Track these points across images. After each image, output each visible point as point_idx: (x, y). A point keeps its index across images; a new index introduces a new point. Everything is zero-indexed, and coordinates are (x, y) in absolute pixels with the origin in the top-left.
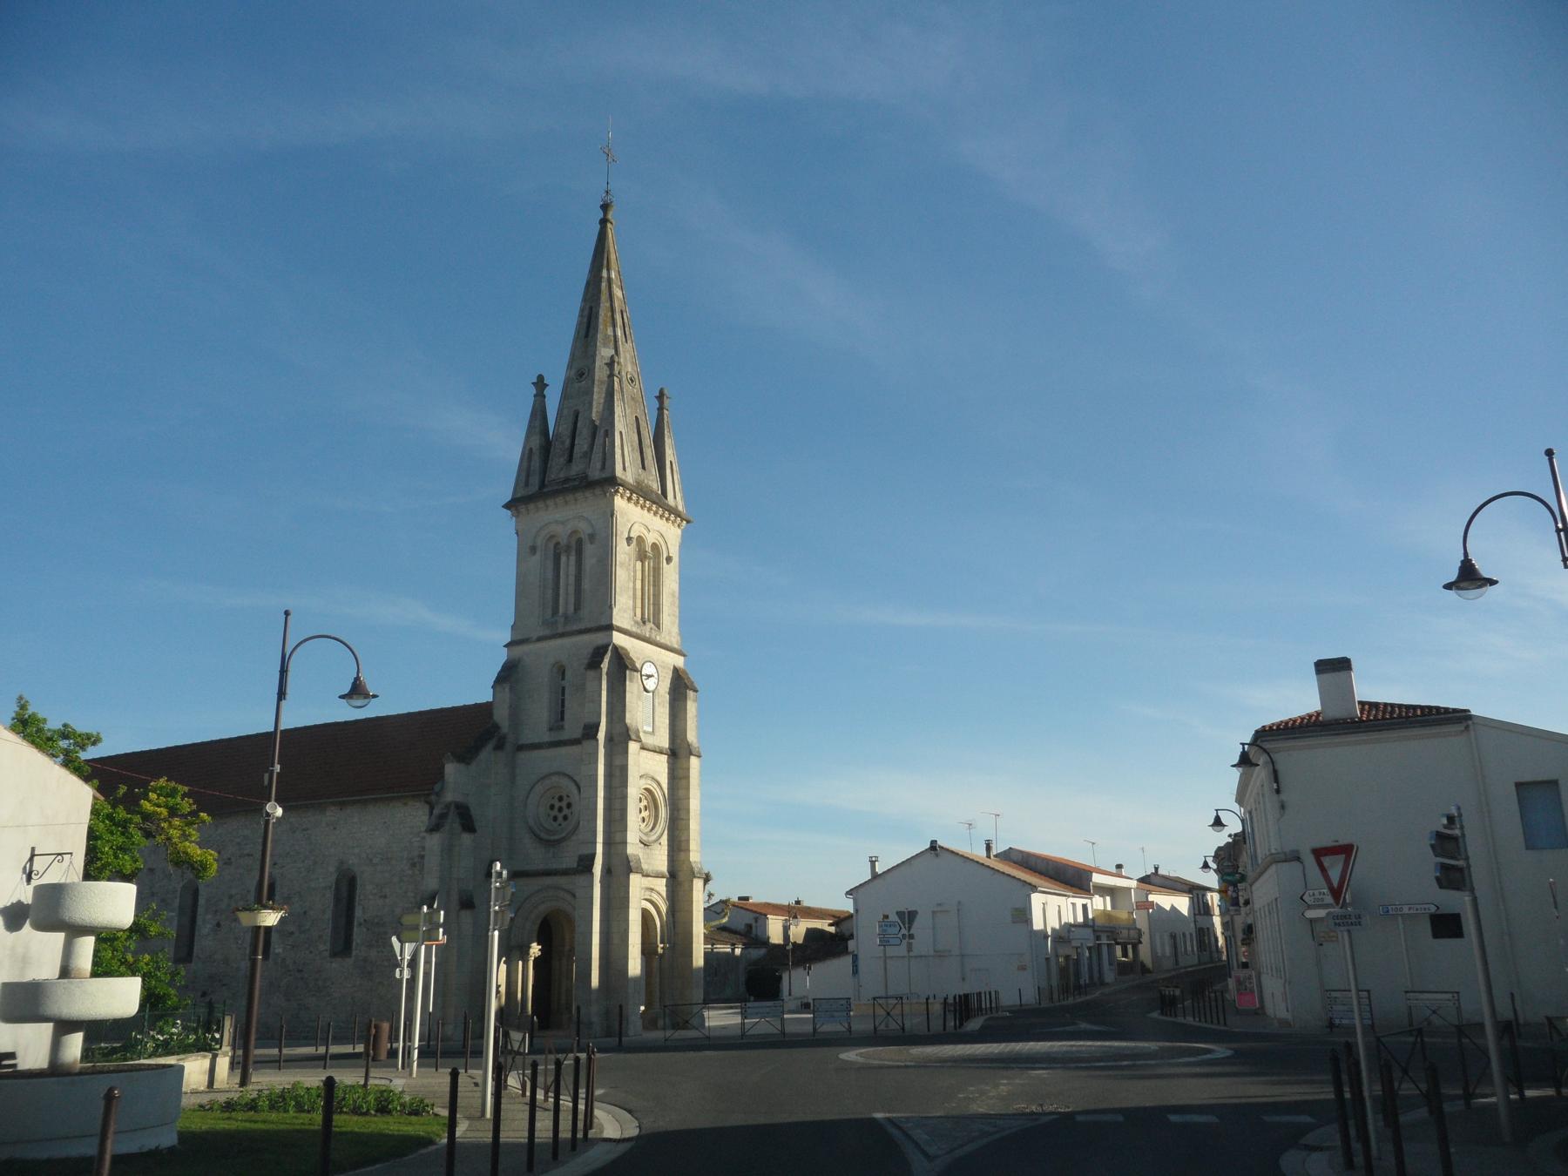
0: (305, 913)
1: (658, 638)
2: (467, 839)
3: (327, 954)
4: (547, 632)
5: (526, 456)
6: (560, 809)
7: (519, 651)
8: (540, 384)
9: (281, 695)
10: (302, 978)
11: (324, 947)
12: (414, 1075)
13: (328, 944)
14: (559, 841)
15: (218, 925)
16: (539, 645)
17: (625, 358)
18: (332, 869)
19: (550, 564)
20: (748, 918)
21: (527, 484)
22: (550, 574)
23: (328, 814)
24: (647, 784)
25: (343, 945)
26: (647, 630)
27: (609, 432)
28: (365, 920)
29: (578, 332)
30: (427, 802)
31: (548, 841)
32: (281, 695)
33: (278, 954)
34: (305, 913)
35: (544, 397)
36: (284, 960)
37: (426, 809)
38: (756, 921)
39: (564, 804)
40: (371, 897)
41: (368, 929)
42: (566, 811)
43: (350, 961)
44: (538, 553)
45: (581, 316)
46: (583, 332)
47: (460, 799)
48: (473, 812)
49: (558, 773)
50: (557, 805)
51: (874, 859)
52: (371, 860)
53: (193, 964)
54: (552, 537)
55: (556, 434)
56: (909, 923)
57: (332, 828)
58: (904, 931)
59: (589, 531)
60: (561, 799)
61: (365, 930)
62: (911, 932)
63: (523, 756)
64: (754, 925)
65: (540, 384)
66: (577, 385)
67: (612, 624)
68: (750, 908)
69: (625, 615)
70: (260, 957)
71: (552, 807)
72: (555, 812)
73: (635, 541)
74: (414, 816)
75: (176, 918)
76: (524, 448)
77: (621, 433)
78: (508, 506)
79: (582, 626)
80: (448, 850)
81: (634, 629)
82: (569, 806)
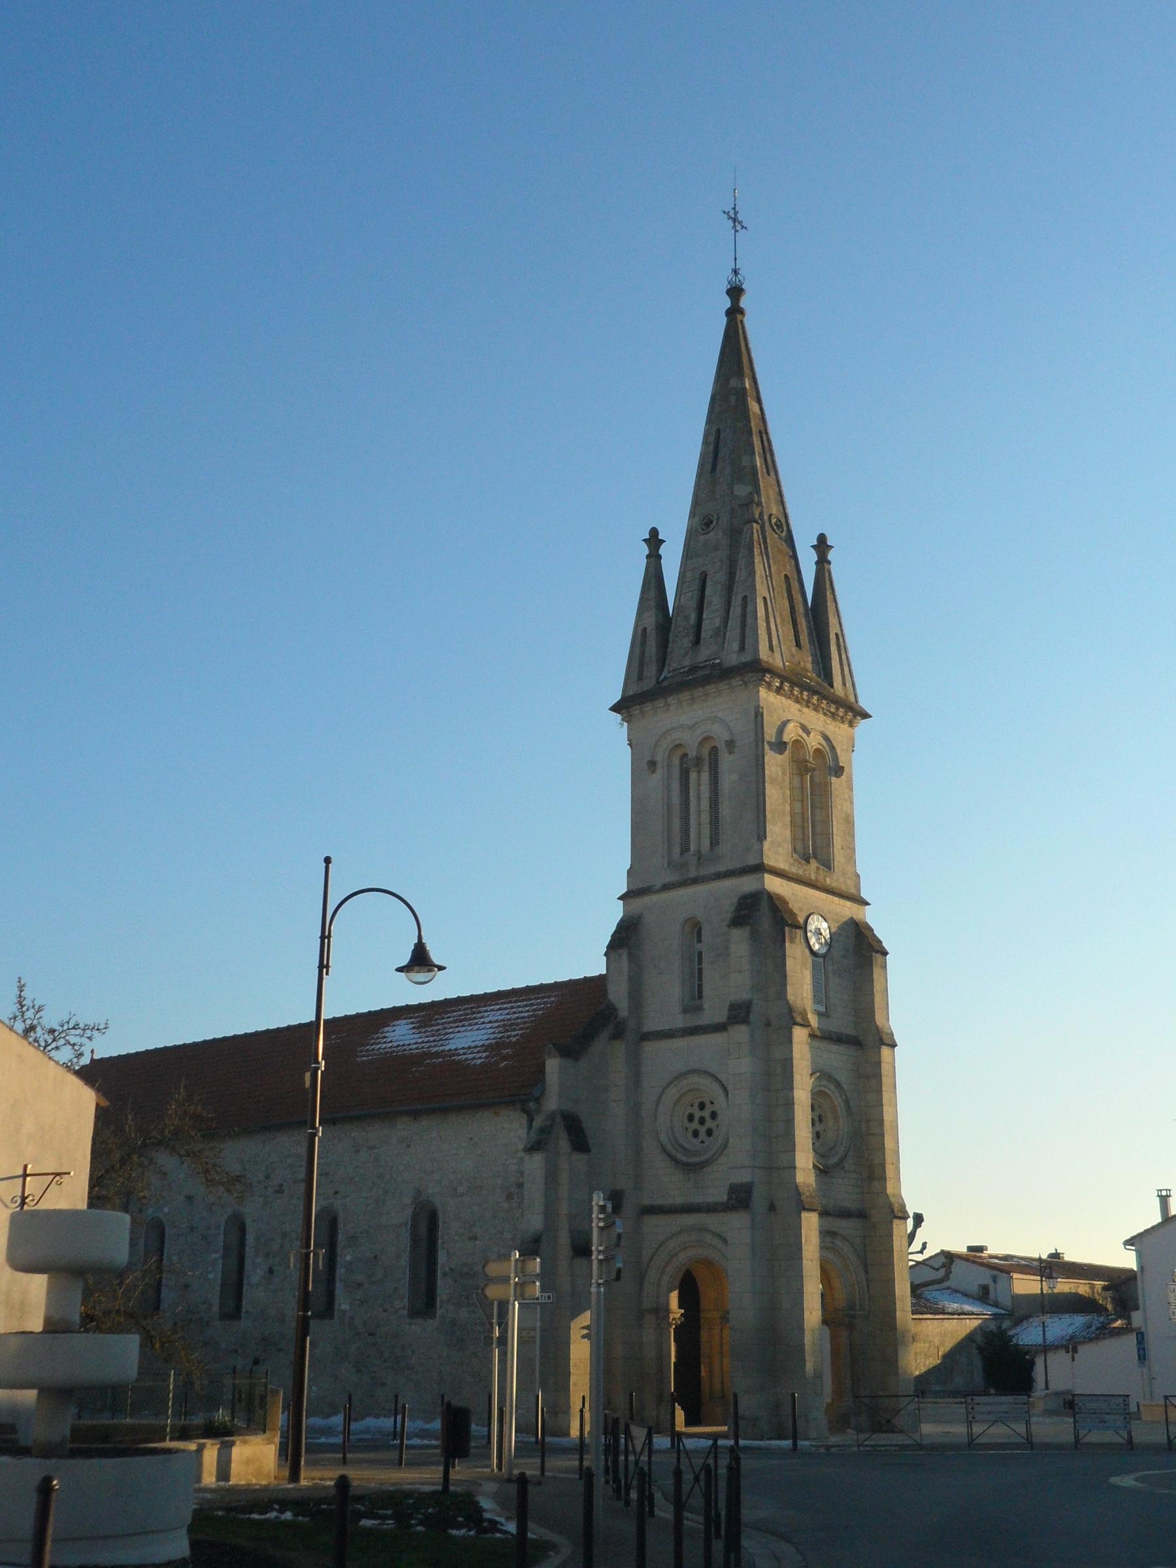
0: (376, 1257)
2: (579, 1159)
3: (404, 1312)
4: (674, 877)
5: (638, 643)
6: (702, 1121)
7: (639, 903)
8: (654, 541)
9: (323, 966)
14: (702, 1165)
15: (271, 1271)
16: (664, 896)
18: (407, 1201)
19: (676, 785)
20: (984, 1277)
21: (640, 678)
26: (812, 870)
29: (701, 466)
30: (526, 1111)
31: (687, 1164)
32: (323, 966)
35: (660, 557)
36: (352, 1318)
37: (524, 1119)
38: (995, 1282)
39: (706, 1114)
42: (709, 1123)
43: (432, 1324)
44: (659, 771)
45: (705, 442)
46: (709, 467)
50: (698, 1114)
51: (1164, 1193)
59: (727, 737)
60: (702, 1106)
63: (649, 1047)
64: (991, 1289)
65: (654, 541)
71: (691, 1118)
72: (695, 1125)
77: (765, 598)
78: (616, 708)
79: (721, 868)
80: (551, 1177)
81: (795, 870)
82: (714, 1115)
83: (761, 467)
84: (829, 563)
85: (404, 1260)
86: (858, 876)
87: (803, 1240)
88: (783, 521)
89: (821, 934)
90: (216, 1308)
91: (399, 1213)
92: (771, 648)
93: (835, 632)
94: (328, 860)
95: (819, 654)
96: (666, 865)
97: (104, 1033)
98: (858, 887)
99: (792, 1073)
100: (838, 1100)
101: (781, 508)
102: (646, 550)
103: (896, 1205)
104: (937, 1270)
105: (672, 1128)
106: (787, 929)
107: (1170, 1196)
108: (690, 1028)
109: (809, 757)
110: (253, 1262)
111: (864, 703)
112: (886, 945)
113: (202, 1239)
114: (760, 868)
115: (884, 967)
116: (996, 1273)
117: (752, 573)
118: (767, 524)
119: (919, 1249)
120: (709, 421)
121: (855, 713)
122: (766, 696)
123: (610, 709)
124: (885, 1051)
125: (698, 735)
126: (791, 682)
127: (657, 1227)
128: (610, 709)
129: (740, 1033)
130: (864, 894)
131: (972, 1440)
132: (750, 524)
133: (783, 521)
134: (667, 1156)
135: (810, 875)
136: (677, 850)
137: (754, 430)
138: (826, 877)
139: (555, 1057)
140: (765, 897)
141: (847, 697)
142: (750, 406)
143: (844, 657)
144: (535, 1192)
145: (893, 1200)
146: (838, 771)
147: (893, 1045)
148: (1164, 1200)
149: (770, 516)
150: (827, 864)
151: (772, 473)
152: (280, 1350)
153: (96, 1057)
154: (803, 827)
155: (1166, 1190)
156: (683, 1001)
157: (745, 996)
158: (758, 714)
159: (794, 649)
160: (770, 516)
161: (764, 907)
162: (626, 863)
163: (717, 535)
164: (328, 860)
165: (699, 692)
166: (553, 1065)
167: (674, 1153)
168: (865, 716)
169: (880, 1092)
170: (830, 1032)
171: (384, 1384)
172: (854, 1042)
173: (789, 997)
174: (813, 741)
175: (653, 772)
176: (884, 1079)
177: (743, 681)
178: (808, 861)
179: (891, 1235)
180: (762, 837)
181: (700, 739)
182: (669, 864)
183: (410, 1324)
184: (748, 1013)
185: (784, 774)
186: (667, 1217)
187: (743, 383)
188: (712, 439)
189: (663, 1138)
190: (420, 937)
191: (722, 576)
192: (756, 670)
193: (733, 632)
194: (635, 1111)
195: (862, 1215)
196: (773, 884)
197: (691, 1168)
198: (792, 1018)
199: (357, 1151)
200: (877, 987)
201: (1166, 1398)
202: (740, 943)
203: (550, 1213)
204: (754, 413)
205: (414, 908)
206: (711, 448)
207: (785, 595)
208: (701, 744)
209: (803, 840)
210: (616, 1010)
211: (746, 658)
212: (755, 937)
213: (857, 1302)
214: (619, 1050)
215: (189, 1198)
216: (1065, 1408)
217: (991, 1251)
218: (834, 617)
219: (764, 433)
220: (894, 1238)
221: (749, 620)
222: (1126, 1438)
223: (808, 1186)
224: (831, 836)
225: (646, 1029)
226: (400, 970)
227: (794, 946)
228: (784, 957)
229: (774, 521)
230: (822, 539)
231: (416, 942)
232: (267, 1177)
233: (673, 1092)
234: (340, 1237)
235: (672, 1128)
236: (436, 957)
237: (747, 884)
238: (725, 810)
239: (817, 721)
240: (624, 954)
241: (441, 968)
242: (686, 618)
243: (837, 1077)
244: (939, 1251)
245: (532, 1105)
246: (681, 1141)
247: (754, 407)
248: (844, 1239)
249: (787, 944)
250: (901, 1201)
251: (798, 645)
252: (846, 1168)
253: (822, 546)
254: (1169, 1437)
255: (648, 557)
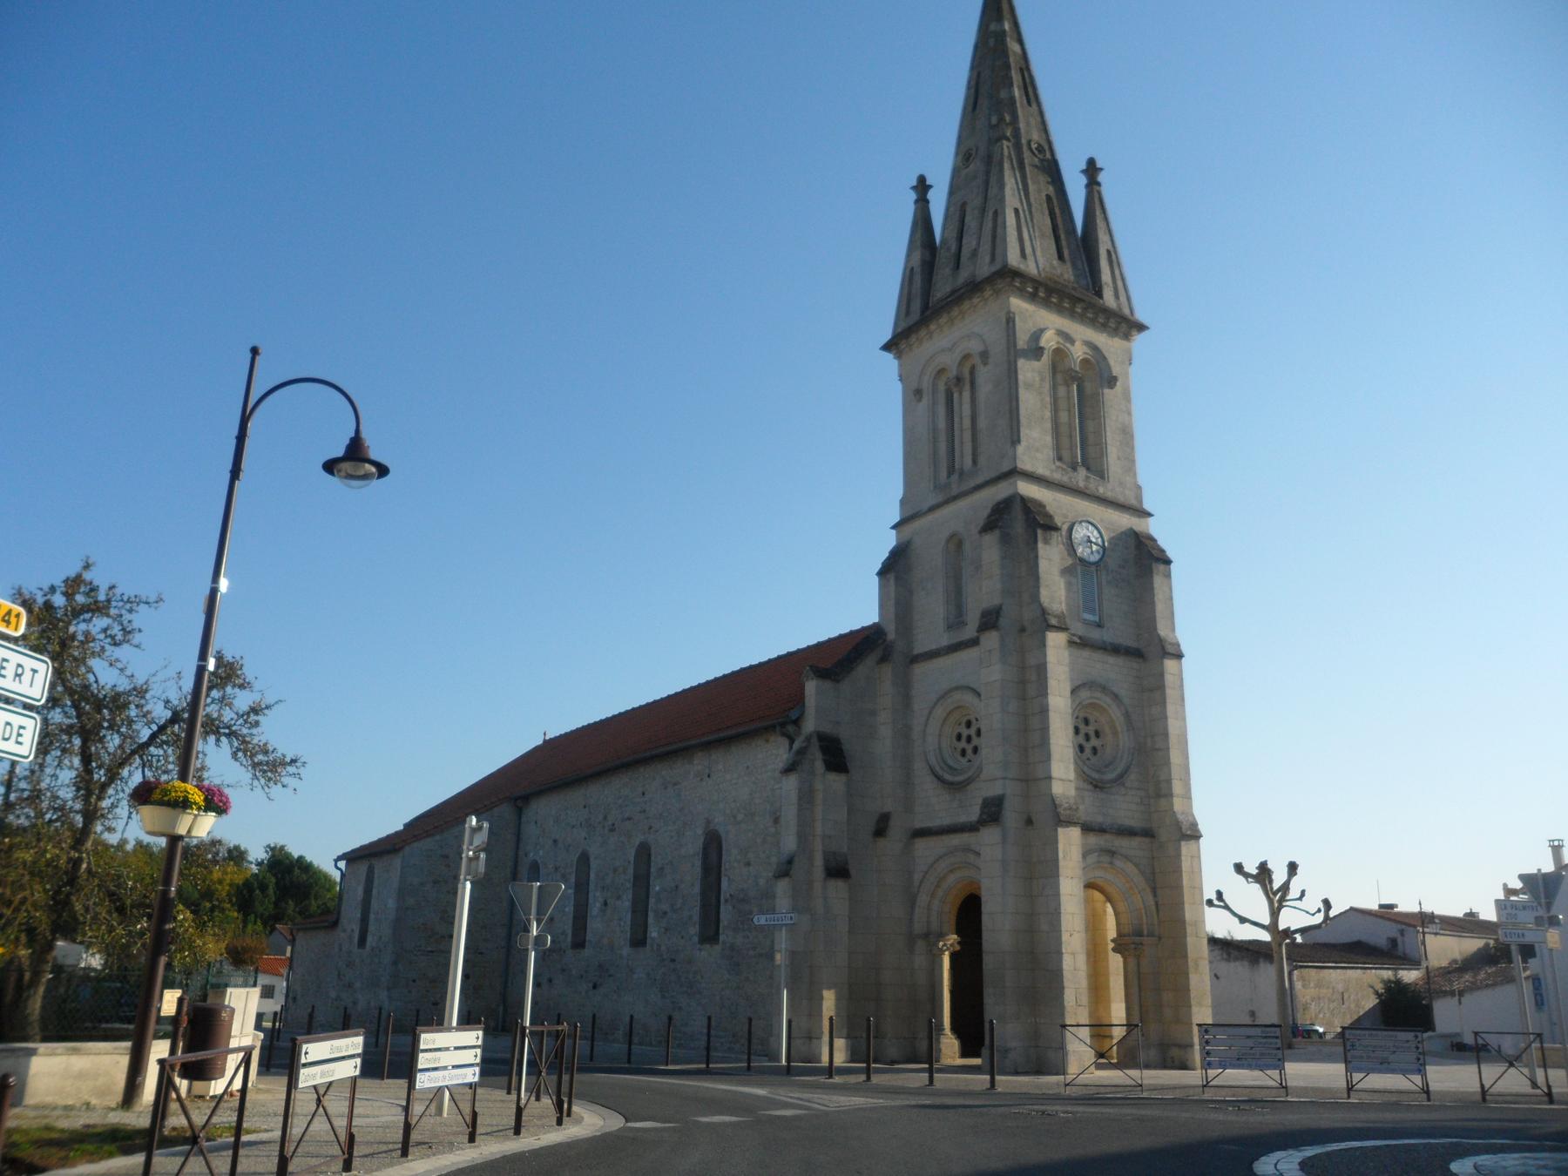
0: (677, 887)
1: (1101, 490)
2: (836, 781)
3: (696, 939)
4: (940, 498)
5: (907, 279)
6: (969, 739)
7: (909, 529)
8: (922, 187)
9: (235, 472)
10: (674, 970)
11: (694, 930)
12: (445, 1115)
13: (697, 926)
14: (969, 781)
15: (606, 904)
16: (930, 517)
17: (1028, 124)
18: (700, 831)
19: (941, 410)
20: (1391, 930)
21: (908, 313)
22: (942, 423)
23: (695, 762)
24: (1091, 698)
25: (710, 934)
26: (1080, 478)
27: (999, 211)
28: (731, 895)
29: (965, 109)
30: (784, 734)
31: (952, 784)
32: (235, 472)
33: (653, 939)
34: (677, 887)
35: (927, 202)
36: (659, 946)
37: (786, 742)
38: (1402, 935)
39: (972, 731)
40: (736, 864)
41: (734, 907)
42: (975, 741)
43: (718, 948)
44: (925, 401)
45: (969, 88)
46: (970, 108)
47: (827, 728)
48: (846, 747)
49: (957, 688)
50: (965, 733)
51: (1556, 843)
52: (735, 817)
53: (586, 950)
54: (941, 371)
55: (943, 241)
56: (1546, 897)
57: (699, 779)
58: (1541, 912)
59: (981, 348)
60: (969, 724)
61: (730, 908)
62: (1552, 913)
63: (919, 670)
64: (1399, 940)
65: (922, 187)
66: (964, 172)
67: (1016, 467)
68: (1393, 918)
69: (1039, 455)
70: (173, 889)
71: (959, 737)
72: (963, 744)
73: (1046, 358)
74: (776, 752)
75: (573, 896)
76: (905, 269)
77: (1016, 211)
78: (887, 347)
79: (980, 479)
80: (806, 797)
81: (1057, 476)
82: (979, 733)
83: (1021, 97)
84: (1099, 184)
85: (697, 889)
86: (1139, 488)
87: (1061, 855)
88: (1046, 147)
89: (1091, 542)
90: (569, 939)
91: (693, 844)
92: (1023, 255)
93: (1106, 248)
94: (255, 351)
95: (1087, 269)
96: (932, 488)
97: (156, 608)
98: (1139, 498)
99: (1046, 678)
100: (1116, 713)
101: (1044, 136)
102: (913, 196)
103: (1185, 823)
104: (1313, 915)
105: (940, 748)
106: (1039, 532)
107: (1563, 846)
108: (953, 645)
109: (1075, 365)
110: (594, 896)
111: (1141, 315)
112: (1170, 554)
113: (535, 872)
114: (1014, 473)
115: (1168, 576)
116: (1404, 927)
117: (1002, 186)
118: (1025, 148)
119: (1298, 896)
120: (973, 68)
121: (1126, 325)
122: (1017, 303)
123: (880, 349)
124: (1169, 664)
125: (957, 355)
126: (1046, 292)
127: (925, 849)
128: (880, 349)
129: (991, 640)
130: (1147, 506)
131: (1208, 1083)
132: (999, 144)
133: (1046, 147)
134: (935, 779)
135: (1077, 482)
136: (944, 474)
137: (1013, 65)
138: (1099, 485)
139: (812, 679)
140: (1019, 500)
141: (1120, 309)
142: (1009, 45)
143: (1117, 272)
144: (790, 814)
145: (1181, 817)
146: (1112, 381)
147: (1179, 656)
148: (1557, 850)
149: (1029, 142)
150: (1101, 475)
151: (1034, 105)
152: (610, 976)
153: (547, 738)
154: (1071, 436)
155: (1559, 840)
156: (948, 618)
157: (996, 601)
158: (1010, 320)
159: (1055, 262)
160: (1029, 142)
161: (1017, 508)
162: (899, 492)
163: (976, 165)
164: (255, 351)
165: (955, 312)
166: (811, 687)
167: (940, 773)
168: (1141, 328)
169: (1163, 703)
170: (1104, 642)
171: (680, 1008)
172: (1136, 653)
173: (1042, 600)
174: (1078, 352)
175: (920, 400)
176: (1169, 692)
177: (994, 290)
178: (1074, 469)
179: (1179, 855)
180: (1016, 441)
181: (959, 359)
182: (935, 487)
183: (700, 950)
184: (997, 618)
185: (1042, 380)
186: (935, 838)
187: (1003, 25)
188: (973, 83)
189: (933, 761)
190: (357, 431)
191: (978, 201)
192: (1008, 276)
193: (986, 248)
194: (904, 735)
195: (1148, 833)
196: (1027, 489)
197: (955, 787)
198: (1046, 620)
199: (666, 788)
200: (1159, 597)
201: (1476, 1034)
202: (990, 550)
203: (803, 836)
204: (1014, 52)
205: (345, 389)
206: (973, 90)
207: (1047, 212)
208: (961, 364)
209: (1071, 449)
210: (885, 635)
211: (997, 266)
212: (1006, 540)
213: (1145, 926)
214: (887, 671)
215: (555, 841)
216: (1453, 1050)
217: (1400, 909)
218: (1105, 233)
219: (1025, 68)
220: (1183, 858)
221: (999, 230)
222: (1421, 1086)
223: (1068, 798)
224: (1104, 446)
225: (916, 652)
226: (330, 467)
227: (1048, 547)
228: (1037, 557)
229: (1034, 146)
230: (1091, 163)
231: (353, 435)
232: (605, 818)
233: (940, 712)
234: (652, 870)
235: (940, 748)
236: (376, 450)
237: (1000, 492)
238: (982, 423)
239: (1083, 333)
240: (891, 577)
241: (383, 471)
242: (948, 249)
243: (1115, 689)
244: (1348, 908)
245: (791, 729)
246: (951, 762)
247: (1014, 47)
248: (1127, 858)
249: (1040, 545)
250: (1191, 818)
251: (1061, 257)
252: (1126, 785)
253: (1092, 170)
254: (1482, 1086)
255: (916, 202)
